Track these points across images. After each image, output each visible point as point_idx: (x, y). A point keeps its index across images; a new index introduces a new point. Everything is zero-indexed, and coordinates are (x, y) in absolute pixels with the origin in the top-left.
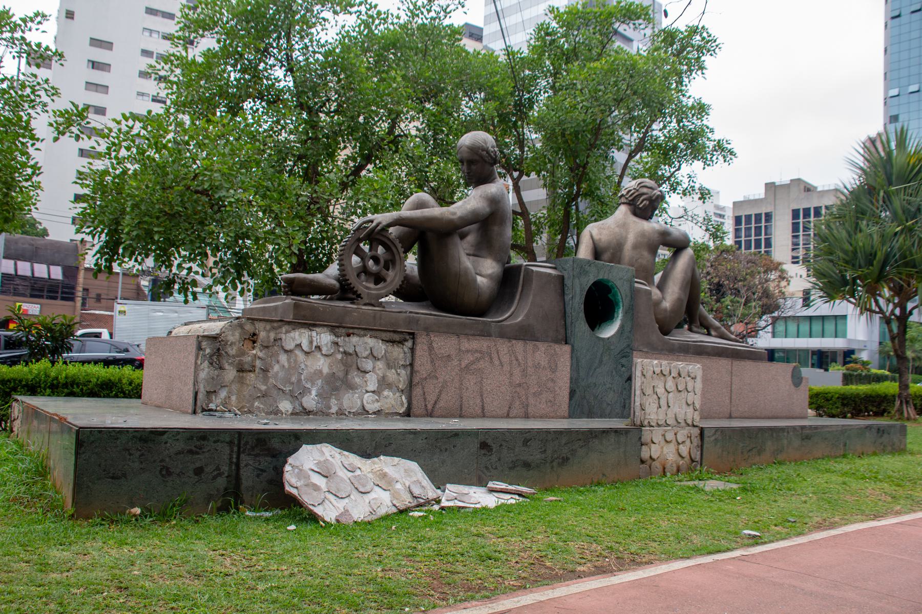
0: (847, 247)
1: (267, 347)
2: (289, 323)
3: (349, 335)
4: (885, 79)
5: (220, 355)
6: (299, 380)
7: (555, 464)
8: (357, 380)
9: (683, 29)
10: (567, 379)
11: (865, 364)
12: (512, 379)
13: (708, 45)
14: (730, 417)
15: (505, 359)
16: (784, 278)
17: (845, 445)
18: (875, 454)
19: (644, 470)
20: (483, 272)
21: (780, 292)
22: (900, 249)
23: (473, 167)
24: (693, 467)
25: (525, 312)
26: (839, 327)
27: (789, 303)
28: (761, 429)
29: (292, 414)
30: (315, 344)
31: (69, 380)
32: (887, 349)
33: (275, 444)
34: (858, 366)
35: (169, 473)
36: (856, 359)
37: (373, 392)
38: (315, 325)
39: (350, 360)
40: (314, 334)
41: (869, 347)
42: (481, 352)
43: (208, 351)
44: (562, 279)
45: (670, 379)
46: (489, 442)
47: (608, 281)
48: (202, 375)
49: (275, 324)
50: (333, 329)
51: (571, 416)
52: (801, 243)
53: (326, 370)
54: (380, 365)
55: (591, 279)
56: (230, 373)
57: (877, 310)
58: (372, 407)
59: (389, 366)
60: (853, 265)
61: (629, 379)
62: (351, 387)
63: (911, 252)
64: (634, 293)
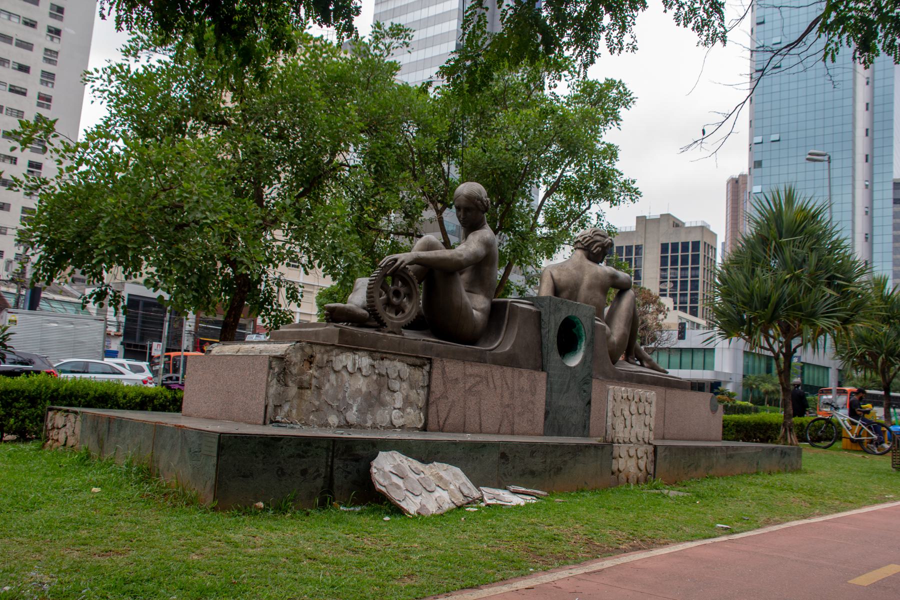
0: (746, 290)
1: (321, 368)
2: (338, 347)
3: (382, 359)
4: (750, 126)
5: (285, 374)
6: (344, 397)
7: (552, 472)
8: (388, 398)
9: (602, 81)
10: (543, 402)
11: (731, 395)
12: (504, 399)
13: (625, 98)
14: (664, 438)
15: (498, 383)
16: (661, 312)
17: (757, 464)
18: (779, 472)
19: (615, 480)
20: (477, 305)
21: (658, 324)
22: (789, 295)
23: (469, 214)
24: (648, 478)
25: (512, 342)
26: (708, 360)
27: (665, 335)
28: (697, 448)
29: (338, 427)
30: (357, 366)
31: (68, 392)
32: (750, 382)
33: (359, 451)
34: (725, 397)
35: (283, 474)
36: (722, 391)
37: (399, 409)
38: (357, 350)
39: (383, 381)
40: (357, 357)
41: (733, 380)
42: (480, 376)
43: (277, 370)
44: (539, 314)
45: (633, 403)
46: (507, 452)
47: (575, 317)
48: (272, 391)
49: (328, 348)
50: (371, 353)
51: (545, 434)
52: (669, 276)
53: (364, 389)
54: (405, 385)
55: (563, 315)
56: (293, 390)
57: (766, 346)
58: (398, 422)
59: (412, 387)
60: (750, 307)
61: (589, 403)
62: (383, 404)
63: (799, 298)
64: (594, 327)
